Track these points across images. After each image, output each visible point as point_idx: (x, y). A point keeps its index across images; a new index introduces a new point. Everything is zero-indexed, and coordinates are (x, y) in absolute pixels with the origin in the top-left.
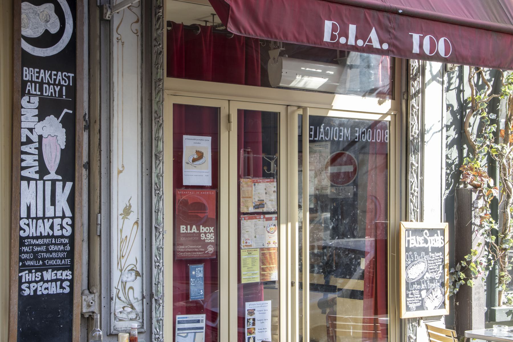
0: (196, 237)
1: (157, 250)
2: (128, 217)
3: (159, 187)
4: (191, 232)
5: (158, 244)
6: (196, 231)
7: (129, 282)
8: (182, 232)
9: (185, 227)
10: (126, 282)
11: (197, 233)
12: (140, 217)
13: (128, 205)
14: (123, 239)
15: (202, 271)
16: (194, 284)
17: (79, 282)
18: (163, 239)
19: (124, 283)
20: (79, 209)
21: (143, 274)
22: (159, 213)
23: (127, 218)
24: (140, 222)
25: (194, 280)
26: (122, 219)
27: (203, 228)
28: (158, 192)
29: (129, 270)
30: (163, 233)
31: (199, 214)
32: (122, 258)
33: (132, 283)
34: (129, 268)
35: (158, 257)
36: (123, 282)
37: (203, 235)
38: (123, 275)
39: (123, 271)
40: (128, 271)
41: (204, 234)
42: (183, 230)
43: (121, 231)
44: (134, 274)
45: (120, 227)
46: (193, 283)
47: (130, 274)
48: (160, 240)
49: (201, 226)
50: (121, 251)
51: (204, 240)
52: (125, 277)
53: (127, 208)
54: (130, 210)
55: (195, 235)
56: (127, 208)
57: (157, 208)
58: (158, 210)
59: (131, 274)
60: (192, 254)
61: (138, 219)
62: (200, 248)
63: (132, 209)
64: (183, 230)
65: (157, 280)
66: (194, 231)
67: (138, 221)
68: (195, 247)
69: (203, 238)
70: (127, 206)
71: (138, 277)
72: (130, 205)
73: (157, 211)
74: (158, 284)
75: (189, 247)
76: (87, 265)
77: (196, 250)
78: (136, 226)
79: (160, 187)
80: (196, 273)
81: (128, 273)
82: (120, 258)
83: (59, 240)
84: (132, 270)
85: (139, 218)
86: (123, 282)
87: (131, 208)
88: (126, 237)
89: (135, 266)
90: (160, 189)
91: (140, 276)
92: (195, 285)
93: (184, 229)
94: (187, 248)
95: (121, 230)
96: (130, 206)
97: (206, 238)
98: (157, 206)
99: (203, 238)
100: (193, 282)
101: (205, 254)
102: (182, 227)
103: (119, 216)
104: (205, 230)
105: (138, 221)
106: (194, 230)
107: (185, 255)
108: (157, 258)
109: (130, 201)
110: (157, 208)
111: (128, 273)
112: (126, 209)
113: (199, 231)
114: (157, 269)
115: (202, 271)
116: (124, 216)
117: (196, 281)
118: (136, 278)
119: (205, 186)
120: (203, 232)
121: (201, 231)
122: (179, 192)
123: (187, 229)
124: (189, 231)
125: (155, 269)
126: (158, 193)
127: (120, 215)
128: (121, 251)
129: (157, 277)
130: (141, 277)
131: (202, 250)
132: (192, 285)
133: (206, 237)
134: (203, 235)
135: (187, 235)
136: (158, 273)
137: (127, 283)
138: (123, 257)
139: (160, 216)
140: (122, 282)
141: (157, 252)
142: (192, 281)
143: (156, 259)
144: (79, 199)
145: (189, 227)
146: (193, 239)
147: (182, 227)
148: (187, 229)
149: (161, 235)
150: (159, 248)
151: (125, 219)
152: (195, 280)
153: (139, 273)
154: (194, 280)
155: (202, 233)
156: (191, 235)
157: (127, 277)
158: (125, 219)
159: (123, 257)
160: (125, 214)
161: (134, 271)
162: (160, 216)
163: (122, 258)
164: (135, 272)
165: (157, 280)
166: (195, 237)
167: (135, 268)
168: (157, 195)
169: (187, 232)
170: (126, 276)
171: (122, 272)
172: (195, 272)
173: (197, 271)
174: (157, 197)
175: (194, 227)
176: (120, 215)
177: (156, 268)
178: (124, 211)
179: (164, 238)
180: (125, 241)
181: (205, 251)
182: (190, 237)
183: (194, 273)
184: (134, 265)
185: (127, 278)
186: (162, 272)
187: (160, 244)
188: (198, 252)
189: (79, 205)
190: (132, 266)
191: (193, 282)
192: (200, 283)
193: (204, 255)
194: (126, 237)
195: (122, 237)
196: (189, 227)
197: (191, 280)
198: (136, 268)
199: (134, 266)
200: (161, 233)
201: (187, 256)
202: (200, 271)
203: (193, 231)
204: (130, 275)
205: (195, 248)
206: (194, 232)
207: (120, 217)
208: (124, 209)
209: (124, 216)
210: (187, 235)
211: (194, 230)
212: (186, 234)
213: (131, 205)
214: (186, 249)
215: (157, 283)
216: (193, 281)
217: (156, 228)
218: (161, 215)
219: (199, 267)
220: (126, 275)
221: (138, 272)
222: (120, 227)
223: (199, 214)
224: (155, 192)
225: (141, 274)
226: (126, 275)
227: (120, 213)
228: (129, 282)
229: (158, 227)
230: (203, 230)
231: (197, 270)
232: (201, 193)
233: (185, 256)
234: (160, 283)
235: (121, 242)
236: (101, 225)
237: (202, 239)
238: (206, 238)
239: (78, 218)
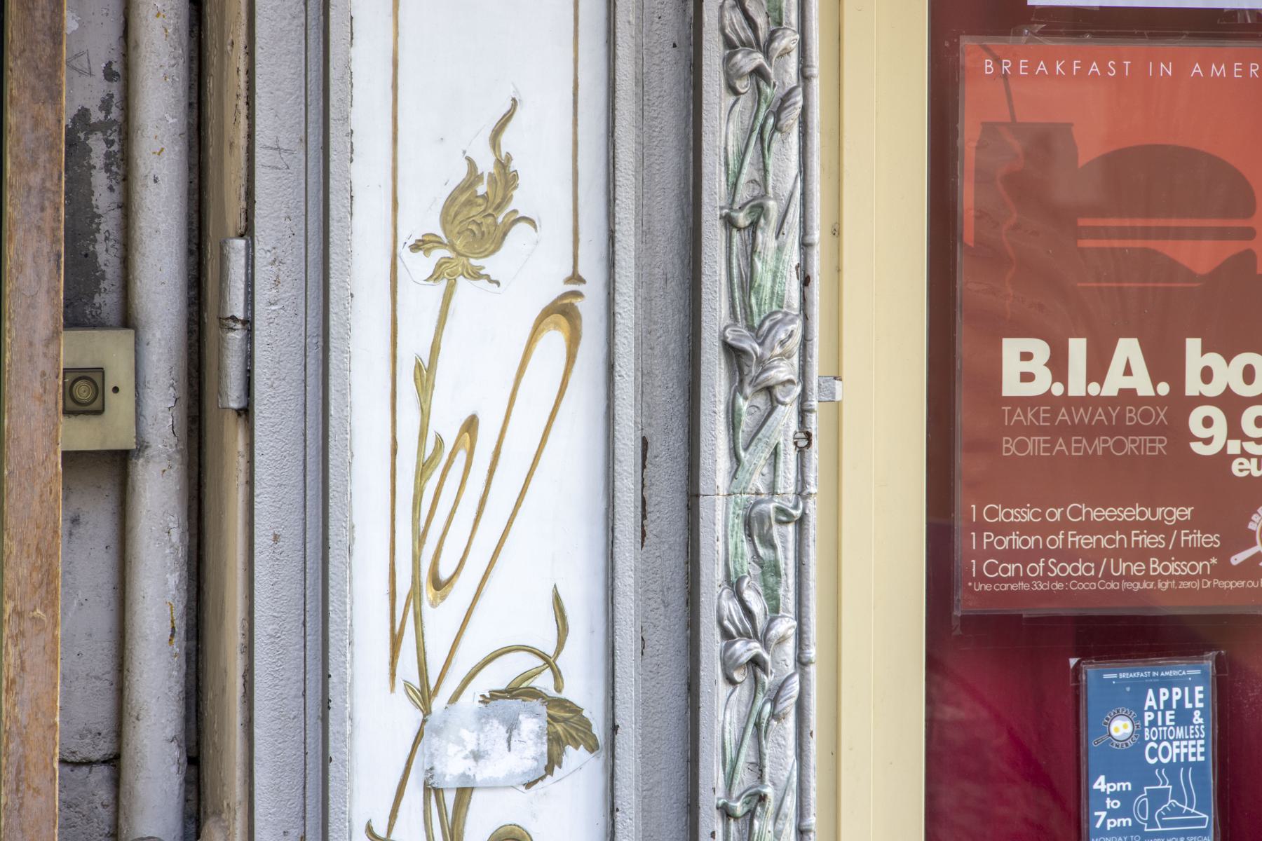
0: (1153, 430)
1: (750, 535)
2: (490, 265)
3: (761, 21)
4: (1094, 389)
5: (758, 482)
6: (1142, 384)
7: (492, 786)
8: (1011, 386)
9: (1041, 349)
10: (464, 794)
11: (1156, 400)
12: (592, 268)
13: (486, 165)
14: (439, 442)
15: (1197, 718)
16: (1126, 821)
17: (37, 780)
18: (801, 452)
19: (450, 798)
20: (34, 201)
21: (615, 728)
22: (766, 239)
23: (476, 275)
24: (590, 309)
25: (1127, 785)
26: (435, 277)
27: (1214, 360)
28: (759, 58)
29: (495, 695)
30: (803, 397)
31: (1167, 248)
32: (428, 592)
33: (522, 796)
34: (498, 676)
35: (749, 595)
36: (438, 791)
37: (1208, 422)
38: (437, 731)
39: (438, 704)
40: (485, 700)
41: (1217, 414)
42: (1027, 377)
43: (425, 376)
44: (531, 725)
45: (414, 344)
46: (1112, 814)
47: (497, 730)
48: (775, 453)
49: (1193, 345)
50: (420, 538)
51: (1224, 458)
52: (452, 749)
53: (482, 189)
54: (499, 207)
55: (1133, 415)
56: (482, 189)
57: (744, 194)
58: (759, 210)
59: (512, 727)
60: (1108, 576)
61: (576, 278)
62: (1180, 525)
63: (520, 201)
64: (1027, 377)
65: (744, 777)
66: (1127, 383)
67: (577, 294)
68: (1134, 513)
69: (1208, 441)
70: (473, 176)
71: (575, 756)
72: (503, 164)
73: (742, 219)
74: (751, 814)
75: (1076, 513)
76: (179, 646)
77: (1146, 540)
78: (554, 341)
79: (778, 23)
80: (1138, 731)
81: (482, 718)
82: (415, 593)
83: (1077, 442)
84: (518, 691)
85: (582, 272)
86: (438, 791)
87: (516, 194)
88: (471, 425)
89: (549, 662)
90: (772, 37)
91: (592, 748)
92: (1137, 828)
93: (1039, 365)
94: (1064, 525)
95: (418, 366)
96: (506, 177)
97: (1234, 447)
98: (748, 172)
99: (1208, 441)
100: (1110, 803)
101: (1224, 571)
102: (1011, 348)
103: (404, 252)
104: (1228, 374)
105: (577, 294)
106: (1128, 371)
107: (1045, 578)
108: (742, 602)
109: (508, 141)
110: (744, 194)
111: (482, 718)
112: (469, 203)
113: (1178, 381)
114: (743, 692)
115: (1197, 718)
116: (446, 253)
117: (1143, 798)
118: (553, 763)
119: (1233, 13)
120: (1214, 390)
121: (1193, 386)
122: (989, 65)
123: (1058, 366)
124: (1078, 385)
125: (723, 689)
126: (759, 73)
127: (416, 247)
128: (420, 538)
129: (747, 754)
130: (602, 754)
131: (1198, 539)
132: (1103, 831)
133: (1235, 431)
134: (1208, 422)
135: (1063, 415)
136: (757, 725)
137: (477, 798)
138: (438, 584)
139: (770, 255)
140: (432, 790)
141: (746, 548)
142: (1103, 795)
143: (731, 607)
144: (37, 122)
145: (1078, 348)
146: (1120, 445)
147: (1011, 348)
148: (1058, 366)
149: (787, 416)
150: (762, 518)
151: (462, 283)
152: (1137, 790)
153: (588, 725)
154: (1127, 785)
155: (1202, 400)
156: (1100, 415)
157: (471, 746)
158: (462, 283)
159: (438, 584)
160: (459, 243)
161: (536, 704)
162: (770, 255)
163: (428, 592)
164: (543, 710)
165: (744, 777)
166: (1137, 430)
167: (544, 682)
168: (742, 85)
169: (1058, 390)
170: (461, 742)
171: (427, 711)
172: (1138, 719)
173: (1148, 717)
174: (745, 102)
175: (1128, 349)
176: (416, 247)
177: (731, 681)
178: (447, 217)
179: (808, 436)
180: (461, 457)
181: (1224, 553)
182: (1091, 432)
183: (1121, 728)
184: (542, 656)
185: (477, 756)
186: (790, 723)
187: (773, 491)
188: (1163, 555)
189: (34, 164)
190: (529, 662)
191: (1110, 803)
192: (1177, 811)
193: (1223, 584)
194: (471, 425)
195: (434, 426)
196: (1078, 348)
197: (1100, 784)
198: (557, 675)
199: (540, 662)
200: (778, 391)
201: (1058, 586)
202: (1183, 717)
203: (1114, 383)
204: (502, 730)
205: (1136, 525)
206: (1128, 395)
207: (418, 266)
208: (452, 199)
209: (446, 253)
210: (1063, 415)
211: (1128, 371)
212: (1055, 413)
213: (514, 166)
214: (1055, 528)
215: (739, 808)
216: (1114, 796)
217: (734, 354)
218: (780, 249)
219: (1169, 683)
220: (465, 734)
221: (577, 711)
222: (414, 344)
223: (1167, 248)
224: (727, 60)
225: (598, 729)
226: (465, 734)
227: (411, 232)
228: (492, 786)
229: (749, 345)
230: (1207, 375)
231: (1150, 702)
232: (1197, 69)
233: (1041, 586)
234: (771, 806)
235: (423, 470)
236: (248, 323)
237: (1197, 448)
238: (1234, 447)
239: (29, 271)
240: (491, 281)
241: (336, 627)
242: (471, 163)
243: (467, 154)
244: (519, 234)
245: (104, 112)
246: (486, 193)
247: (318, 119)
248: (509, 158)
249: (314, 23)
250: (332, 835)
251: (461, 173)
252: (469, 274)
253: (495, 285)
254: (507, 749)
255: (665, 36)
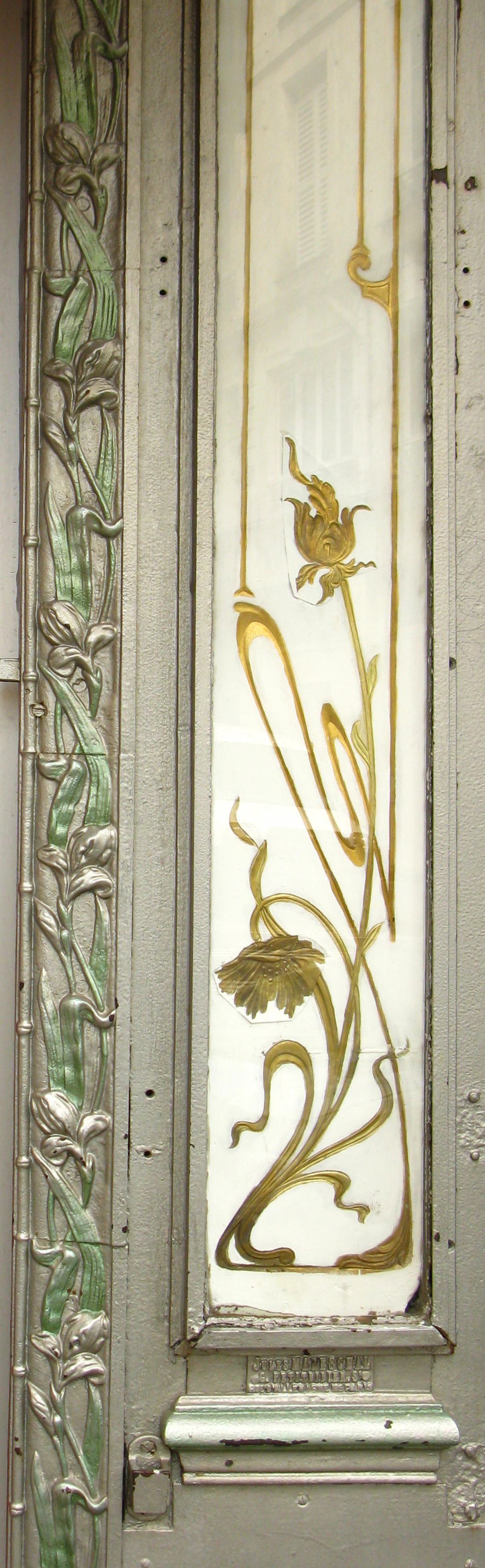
13: (303, 494)
23: (354, 569)
26: (328, 592)
70: (301, 511)
178: (305, 548)
240: (366, 566)
241: (438, 841)
242: (293, 501)
243: (284, 498)
244: (359, 519)
245: (85, 871)
246: (318, 512)
247: (187, 653)
248: (314, 477)
249: (183, 792)
250: (246, 2)
251: (290, 508)
252: (350, 573)
253: (371, 567)
254: (454, 372)
255: (443, 564)
